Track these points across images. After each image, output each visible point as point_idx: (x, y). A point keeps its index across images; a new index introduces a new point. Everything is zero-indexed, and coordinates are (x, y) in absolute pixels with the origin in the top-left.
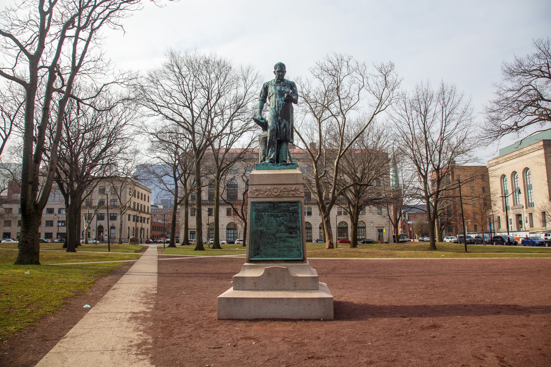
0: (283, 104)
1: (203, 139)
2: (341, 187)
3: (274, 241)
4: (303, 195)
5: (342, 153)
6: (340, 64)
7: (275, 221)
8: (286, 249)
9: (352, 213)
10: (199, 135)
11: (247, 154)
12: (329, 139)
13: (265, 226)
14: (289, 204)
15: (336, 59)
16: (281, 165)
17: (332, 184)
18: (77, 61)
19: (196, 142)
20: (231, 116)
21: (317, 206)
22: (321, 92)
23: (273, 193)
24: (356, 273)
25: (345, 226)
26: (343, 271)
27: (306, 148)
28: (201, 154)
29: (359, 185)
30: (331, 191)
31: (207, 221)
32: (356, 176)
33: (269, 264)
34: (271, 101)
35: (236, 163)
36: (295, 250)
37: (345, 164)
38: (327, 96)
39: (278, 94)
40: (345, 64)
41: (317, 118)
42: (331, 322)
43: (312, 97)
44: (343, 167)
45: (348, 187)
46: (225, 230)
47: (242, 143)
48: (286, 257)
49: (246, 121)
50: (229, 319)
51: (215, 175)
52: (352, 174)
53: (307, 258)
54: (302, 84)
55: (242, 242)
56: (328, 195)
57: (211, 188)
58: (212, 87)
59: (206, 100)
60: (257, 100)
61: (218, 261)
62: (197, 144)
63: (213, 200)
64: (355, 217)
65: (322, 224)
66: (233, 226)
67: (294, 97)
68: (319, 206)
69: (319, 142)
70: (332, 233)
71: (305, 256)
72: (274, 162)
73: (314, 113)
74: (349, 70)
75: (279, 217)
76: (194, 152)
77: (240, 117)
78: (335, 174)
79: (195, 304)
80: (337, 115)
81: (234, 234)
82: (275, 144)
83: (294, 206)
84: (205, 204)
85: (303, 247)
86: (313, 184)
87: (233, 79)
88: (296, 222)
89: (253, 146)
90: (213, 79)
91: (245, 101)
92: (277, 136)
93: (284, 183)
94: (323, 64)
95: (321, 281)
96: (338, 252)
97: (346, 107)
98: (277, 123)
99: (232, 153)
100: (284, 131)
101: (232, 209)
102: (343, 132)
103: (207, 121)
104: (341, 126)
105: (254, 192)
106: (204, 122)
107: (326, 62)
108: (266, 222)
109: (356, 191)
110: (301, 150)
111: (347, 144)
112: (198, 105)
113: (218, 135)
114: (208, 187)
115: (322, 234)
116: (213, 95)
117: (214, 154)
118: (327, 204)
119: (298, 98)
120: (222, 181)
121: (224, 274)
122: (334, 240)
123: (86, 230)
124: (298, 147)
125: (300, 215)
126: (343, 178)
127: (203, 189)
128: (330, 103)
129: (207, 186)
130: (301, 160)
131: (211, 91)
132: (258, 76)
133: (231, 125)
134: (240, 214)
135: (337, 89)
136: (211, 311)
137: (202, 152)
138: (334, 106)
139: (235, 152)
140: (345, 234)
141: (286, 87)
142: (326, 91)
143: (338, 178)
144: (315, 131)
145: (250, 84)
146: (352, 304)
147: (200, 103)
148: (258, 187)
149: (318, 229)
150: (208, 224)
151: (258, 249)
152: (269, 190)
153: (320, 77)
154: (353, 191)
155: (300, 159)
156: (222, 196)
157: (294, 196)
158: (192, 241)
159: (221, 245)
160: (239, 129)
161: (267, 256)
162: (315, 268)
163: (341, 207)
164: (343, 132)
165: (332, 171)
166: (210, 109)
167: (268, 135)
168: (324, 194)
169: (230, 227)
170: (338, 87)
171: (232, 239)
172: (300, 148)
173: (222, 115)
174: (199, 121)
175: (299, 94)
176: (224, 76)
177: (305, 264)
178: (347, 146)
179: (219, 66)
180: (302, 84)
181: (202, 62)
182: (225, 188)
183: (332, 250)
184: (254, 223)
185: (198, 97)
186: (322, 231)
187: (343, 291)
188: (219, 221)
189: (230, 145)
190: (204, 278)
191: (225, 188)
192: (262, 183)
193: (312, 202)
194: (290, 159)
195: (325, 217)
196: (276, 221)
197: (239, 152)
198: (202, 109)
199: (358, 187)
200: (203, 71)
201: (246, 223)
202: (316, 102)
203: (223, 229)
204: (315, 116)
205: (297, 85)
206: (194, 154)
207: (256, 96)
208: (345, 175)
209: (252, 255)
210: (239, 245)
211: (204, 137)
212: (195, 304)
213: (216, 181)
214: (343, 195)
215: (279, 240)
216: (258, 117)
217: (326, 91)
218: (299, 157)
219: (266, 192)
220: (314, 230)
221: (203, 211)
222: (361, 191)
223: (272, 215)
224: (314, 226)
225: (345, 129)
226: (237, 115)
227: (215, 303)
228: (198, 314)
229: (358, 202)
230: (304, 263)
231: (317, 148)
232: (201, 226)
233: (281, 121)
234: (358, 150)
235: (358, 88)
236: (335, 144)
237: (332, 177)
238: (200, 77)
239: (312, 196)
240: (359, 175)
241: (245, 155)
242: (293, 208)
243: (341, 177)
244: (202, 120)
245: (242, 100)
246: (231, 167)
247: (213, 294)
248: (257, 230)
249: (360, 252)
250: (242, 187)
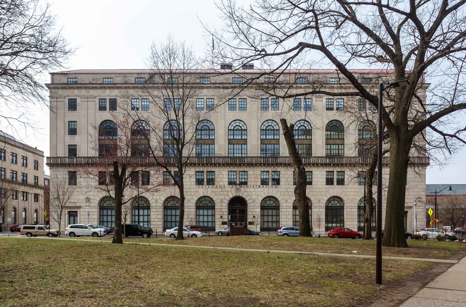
25: (338, 205)
149: (291, 210)
169: (201, 205)
203: (287, 207)
220: (283, 210)
224: (283, 204)
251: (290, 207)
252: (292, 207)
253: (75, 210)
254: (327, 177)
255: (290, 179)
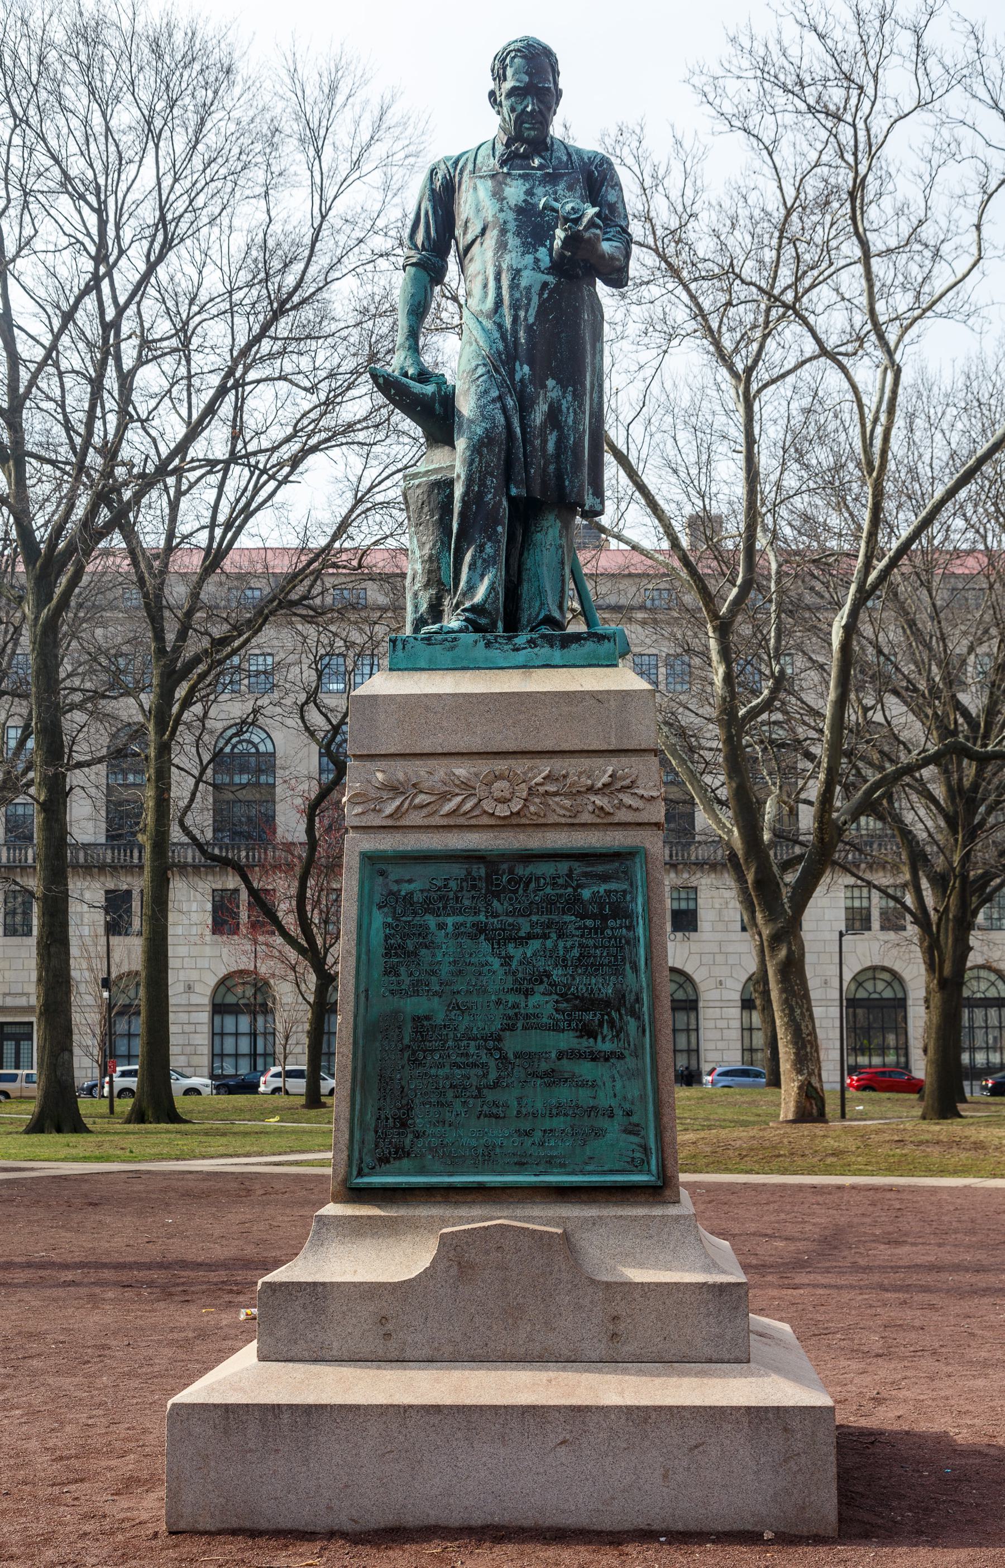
0: (545, 285)
1: (73, 489)
2: (868, 772)
3: (493, 1075)
4: (658, 813)
5: (873, 575)
6: (873, 46)
7: (496, 963)
8: (559, 1123)
9: (934, 917)
10: (47, 468)
11: (329, 582)
12: (798, 493)
13: (439, 994)
14: (579, 868)
15: (849, 16)
16: (532, 643)
17: (817, 750)
18: (254, 505)
19: (33, 508)
20: (235, 361)
21: (728, 879)
22: (757, 213)
23: (488, 806)
24: (957, 1268)
25: (888, 994)
26: (883, 1253)
27: (665, 545)
28: (64, 580)
29: (972, 756)
30: (813, 790)
31: (100, 966)
32: (959, 707)
33: (463, 1212)
34: (472, 268)
35: (268, 636)
36: (613, 1129)
37: (893, 635)
38: (793, 241)
39: (512, 226)
40: (905, 40)
41: (731, 368)
42: (822, 1551)
43: (706, 246)
44: (880, 652)
45: (909, 770)
46: (204, 1017)
47: (297, 516)
48: (563, 1167)
49: (324, 386)
50: (234, 1532)
51: (147, 699)
52: (934, 692)
53: (683, 1177)
54: (648, 170)
55: (298, 1086)
56: (794, 813)
57: (125, 773)
58: (123, 187)
59: (89, 266)
60: (382, 263)
61: (165, 1190)
62: (39, 520)
63: (131, 845)
64: (948, 942)
65: (759, 980)
66: (250, 992)
67: (606, 246)
68: (741, 879)
69: (741, 508)
70: (813, 1033)
71: (670, 1162)
72: (492, 627)
73: (717, 343)
74: (924, 81)
75: (522, 941)
76: (21, 568)
77: (288, 367)
78: (832, 696)
79: (33, 1444)
80: (850, 348)
81: (253, 1035)
82: (497, 522)
83: (605, 878)
84: (92, 869)
85: (658, 1116)
86: (708, 755)
87: (246, 141)
88: (619, 972)
89: (362, 535)
90: (126, 140)
91: (312, 270)
92: (508, 478)
93: (549, 745)
94: (774, 48)
95: (761, 1311)
96: (850, 1143)
97: (903, 301)
98: (510, 402)
99: (241, 577)
100: (551, 446)
101: (244, 895)
102: (884, 452)
103: (97, 385)
104: (869, 417)
105: (380, 800)
106: (78, 394)
107: (791, 32)
108: (445, 970)
109: (954, 792)
110: (637, 558)
111: (905, 522)
112: (41, 292)
113: (162, 470)
114: (102, 768)
115: (759, 1039)
116: (127, 234)
117: (141, 581)
118: (787, 865)
119: (628, 255)
120: (185, 737)
121: (199, 1266)
122: (830, 1075)
124: (619, 537)
125: (640, 931)
126: (878, 717)
127: (75, 778)
128: (807, 282)
129: (100, 760)
130: (640, 615)
131: (119, 213)
132: (389, 119)
133: (238, 409)
134: (290, 921)
135: (852, 195)
136: (129, 1485)
137: (70, 568)
138: (834, 297)
139: (260, 568)
141: (561, 187)
142: (789, 212)
143: (852, 716)
144: (722, 448)
145: (344, 168)
146: (942, 1442)
147: (51, 281)
148: (401, 771)
149: (735, 1012)
150: (106, 983)
151: (403, 1124)
152: (466, 785)
153: (750, 124)
154: (939, 791)
155: (632, 608)
156: (188, 821)
157: (605, 821)
158: (13, 1078)
159: (182, 1104)
160: (282, 436)
161: (454, 1163)
162: (722, 1234)
163: (869, 884)
164: (884, 452)
165: (814, 675)
166: (110, 314)
167: (460, 470)
168: (770, 808)
169: (231, 999)
170: (856, 192)
171: (244, 1069)
172: (635, 548)
173: (184, 349)
174: (48, 383)
175: (636, 229)
176: (193, 119)
177: (672, 1211)
178: (904, 533)
179: (160, 57)
180: (648, 170)
181: (59, 36)
182: (203, 772)
183: (818, 1129)
184: (377, 973)
185: (38, 244)
186: (756, 1018)
187: (885, 1370)
188: (172, 963)
189: (228, 525)
190: (83, 1291)
191: (203, 772)
192: (426, 746)
193: (701, 853)
194: (586, 614)
195: (776, 939)
196: (507, 960)
197: (282, 566)
198: (68, 317)
199: (970, 769)
200: (67, 91)
201: (326, 980)
202: (730, 273)
203: (191, 1008)
204: (724, 358)
205: (624, 176)
206: (23, 580)
207: (379, 243)
208: (891, 701)
209: (368, 1159)
210: (280, 1099)
211: (77, 479)
212: (33, 1444)
213: (152, 736)
214: (881, 818)
215: (519, 1073)
216: (397, 363)
217: (789, 212)
218: (628, 594)
219: (445, 797)
221: (75, 908)
222: (987, 793)
223: (481, 929)
224: (708, 994)
225: (898, 434)
226: (271, 356)
227: (150, 1439)
228: (54, 1501)
229: (966, 858)
230: (665, 1203)
231: (729, 544)
232: (68, 993)
233: (531, 389)
234: (970, 552)
235: (974, 187)
236: (834, 521)
237: (817, 714)
238: (47, 124)
239: (702, 819)
240: (973, 700)
241: (317, 589)
242: (602, 888)
243: (866, 709)
244: (69, 381)
245: (298, 267)
246: (234, 652)
247: (135, 1383)
248: (396, 1014)
249: (979, 1146)
250: (302, 770)
251: (732, 1004)
252: (739, 1004)
253: (26, 1019)
254: (849, 903)
255: (731, 912)
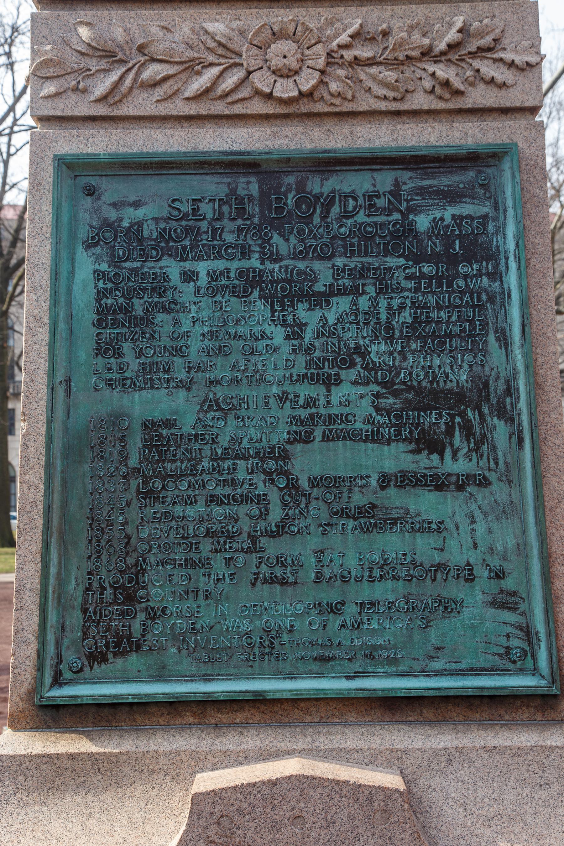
105: (86, 73)
123: (355, 519)
140: (411, 263)
